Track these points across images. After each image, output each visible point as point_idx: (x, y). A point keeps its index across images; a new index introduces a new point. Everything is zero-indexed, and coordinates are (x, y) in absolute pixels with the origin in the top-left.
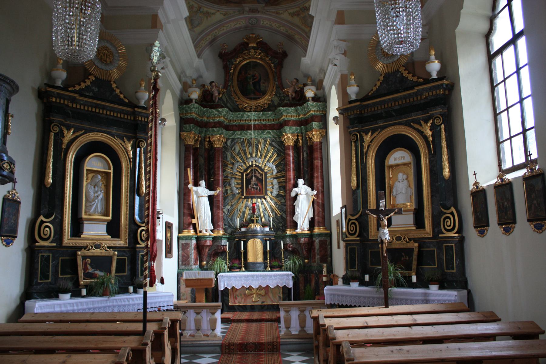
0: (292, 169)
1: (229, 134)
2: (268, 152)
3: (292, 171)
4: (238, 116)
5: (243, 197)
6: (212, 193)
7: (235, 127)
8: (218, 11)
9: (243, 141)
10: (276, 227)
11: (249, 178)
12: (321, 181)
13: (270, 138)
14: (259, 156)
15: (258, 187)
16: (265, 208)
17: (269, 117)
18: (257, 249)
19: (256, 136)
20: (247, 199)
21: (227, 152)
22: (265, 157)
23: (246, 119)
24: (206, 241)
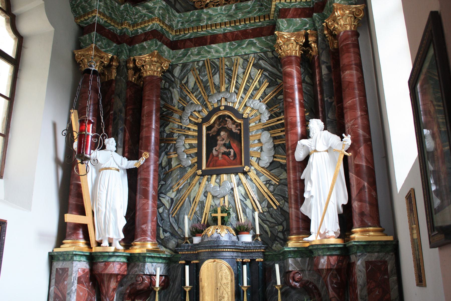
0: (297, 102)
1: (177, 56)
2: (251, 81)
3: (297, 106)
4: (191, 18)
5: (200, 172)
6: (132, 164)
7: (188, 43)
9: (204, 65)
10: (269, 233)
11: (214, 134)
12: (361, 115)
13: (255, 53)
14: (233, 89)
15: (232, 151)
16: (246, 194)
17: (249, 12)
18: (219, 285)
19: (227, 53)
20: (209, 176)
21: (173, 88)
22: (246, 90)
23: (207, 23)
24: (107, 264)
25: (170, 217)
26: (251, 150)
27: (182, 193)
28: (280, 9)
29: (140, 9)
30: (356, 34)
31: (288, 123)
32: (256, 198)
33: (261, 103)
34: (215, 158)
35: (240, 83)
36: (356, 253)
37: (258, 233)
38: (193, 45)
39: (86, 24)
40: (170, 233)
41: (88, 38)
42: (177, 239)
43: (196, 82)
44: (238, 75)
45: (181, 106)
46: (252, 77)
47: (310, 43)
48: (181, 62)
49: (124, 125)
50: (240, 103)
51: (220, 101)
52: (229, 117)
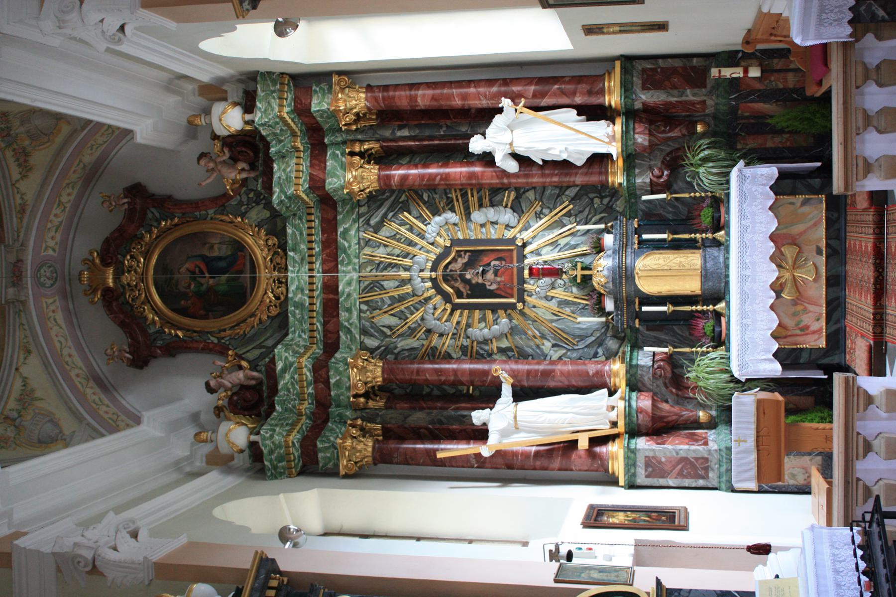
0: (442, 170)
1: (349, 342)
2: (398, 236)
3: (447, 170)
4: (298, 316)
5: (520, 306)
6: (507, 391)
7: (330, 326)
8: (17, 369)
9: (366, 303)
10: (603, 215)
11: (468, 287)
12: (475, 87)
13: (358, 230)
14: (407, 262)
17: (301, 234)
18: (666, 268)
19: (354, 269)
20: (526, 293)
21: (396, 347)
22: (411, 243)
24: (640, 411)
25: (576, 348)
26: (494, 237)
27: (546, 332)
28: (309, 187)
29: (282, 383)
30: (369, 88)
31: (469, 182)
32: (557, 232)
33: (432, 223)
34: (502, 286)
35: (400, 251)
36: (633, 99)
37: (602, 226)
38: (335, 319)
39: (299, 461)
40: (598, 348)
41: (323, 454)
42: (606, 337)
43: (391, 315)
44: (388, 255)
45: (424, 336)
46: (392, 234)
47: (363, 150)
48: (358, 338)
49: (449, 410)
50: (428, 252)
51: (423, 280)
52: (446, 266)
